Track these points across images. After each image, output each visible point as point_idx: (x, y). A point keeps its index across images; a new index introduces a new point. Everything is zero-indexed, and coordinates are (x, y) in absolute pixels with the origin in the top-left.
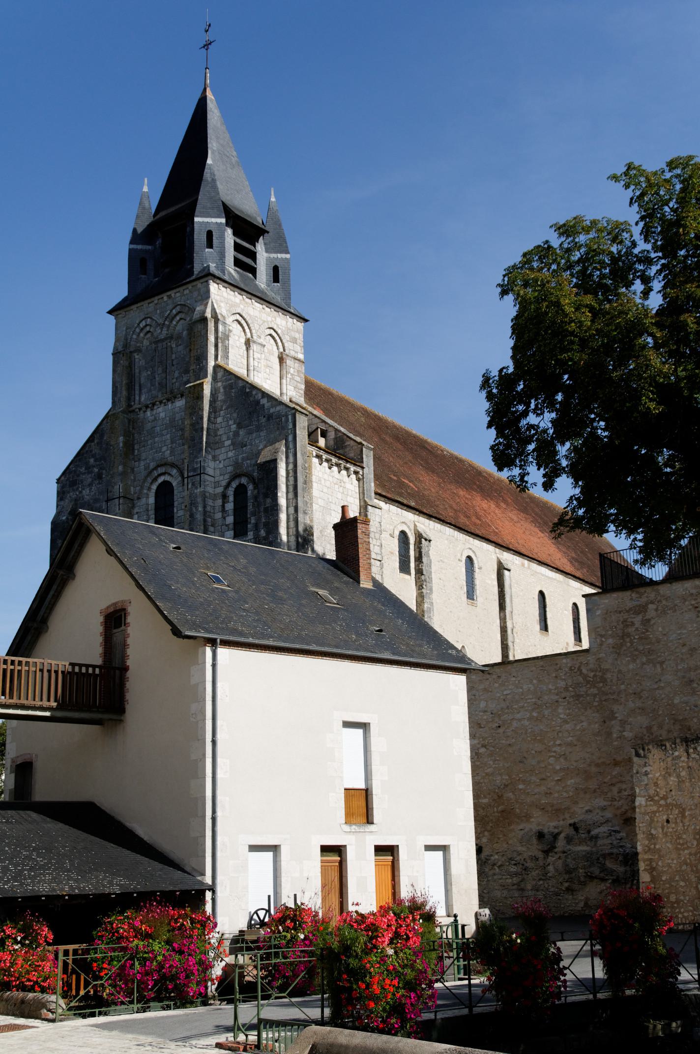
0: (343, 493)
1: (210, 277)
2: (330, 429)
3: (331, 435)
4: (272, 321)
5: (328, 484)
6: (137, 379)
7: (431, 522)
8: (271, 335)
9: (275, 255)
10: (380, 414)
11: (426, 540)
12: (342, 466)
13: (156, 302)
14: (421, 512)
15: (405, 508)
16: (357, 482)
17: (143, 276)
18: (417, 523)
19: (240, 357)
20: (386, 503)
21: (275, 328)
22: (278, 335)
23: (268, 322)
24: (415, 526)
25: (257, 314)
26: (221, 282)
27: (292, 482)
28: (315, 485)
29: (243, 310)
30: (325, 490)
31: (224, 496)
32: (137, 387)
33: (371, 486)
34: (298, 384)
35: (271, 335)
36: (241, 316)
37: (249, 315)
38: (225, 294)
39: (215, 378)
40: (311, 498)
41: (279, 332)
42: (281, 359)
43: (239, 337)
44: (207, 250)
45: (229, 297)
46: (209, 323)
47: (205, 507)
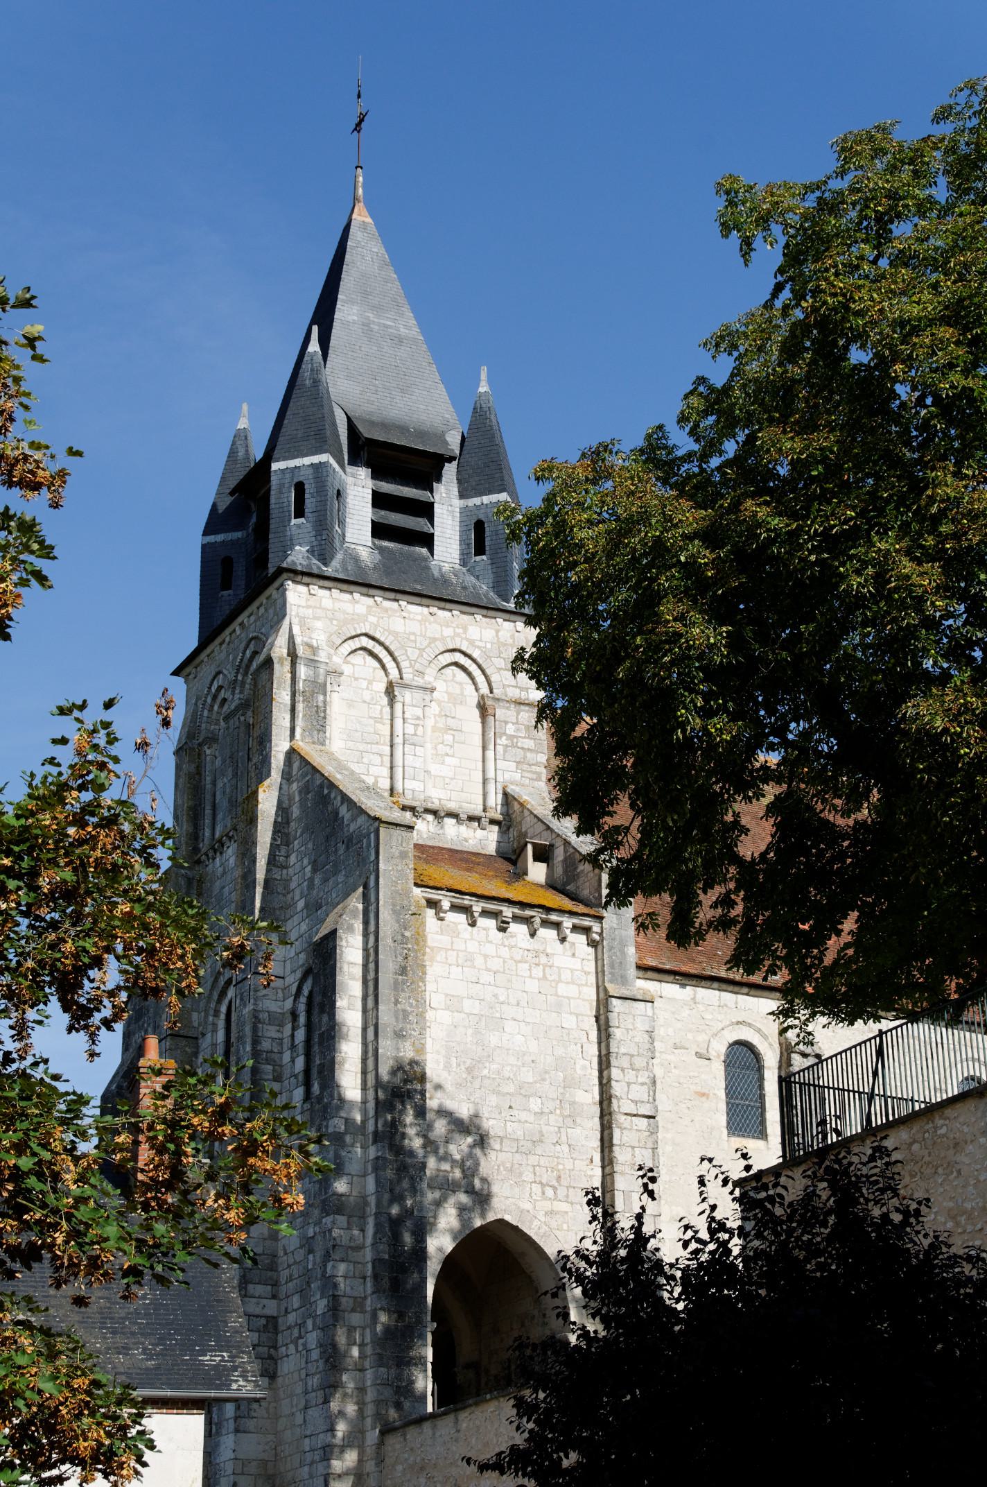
0: (545, 977)
1: (285, 575)
2: (558, 843)
3: (559, 855)
5: (495, 964)
6: (208, 796)
8: (456, 664)
9: (476, 501)
12: (537, 921)
13: (227, 639)
15: (745, 990)
16: (591, 950)
17: (225, 593)
19: (372, 721)
20: (683, 986)
21: (464, 649)
22: (474, 661)
23: (443, 639)
25: (414, 627)
26: (314, 580)
27: (371, 975)
28: (434, 971)
29: (376, 626)
30: (487, 978)
31: (294, 1015)
32: (208, 812)
33: (624, 954)
34: (529, 755)
35: (456, 664)
36: (373, 638)
37: (396, 634)
39: (287, 776)
40: (421, 1002)
41: (475, 655)
42: (483, 709)
43: (370, 682)
44: (294, 521)
45: (338, 605)
46: (276, 666)
47: (256, 1042)
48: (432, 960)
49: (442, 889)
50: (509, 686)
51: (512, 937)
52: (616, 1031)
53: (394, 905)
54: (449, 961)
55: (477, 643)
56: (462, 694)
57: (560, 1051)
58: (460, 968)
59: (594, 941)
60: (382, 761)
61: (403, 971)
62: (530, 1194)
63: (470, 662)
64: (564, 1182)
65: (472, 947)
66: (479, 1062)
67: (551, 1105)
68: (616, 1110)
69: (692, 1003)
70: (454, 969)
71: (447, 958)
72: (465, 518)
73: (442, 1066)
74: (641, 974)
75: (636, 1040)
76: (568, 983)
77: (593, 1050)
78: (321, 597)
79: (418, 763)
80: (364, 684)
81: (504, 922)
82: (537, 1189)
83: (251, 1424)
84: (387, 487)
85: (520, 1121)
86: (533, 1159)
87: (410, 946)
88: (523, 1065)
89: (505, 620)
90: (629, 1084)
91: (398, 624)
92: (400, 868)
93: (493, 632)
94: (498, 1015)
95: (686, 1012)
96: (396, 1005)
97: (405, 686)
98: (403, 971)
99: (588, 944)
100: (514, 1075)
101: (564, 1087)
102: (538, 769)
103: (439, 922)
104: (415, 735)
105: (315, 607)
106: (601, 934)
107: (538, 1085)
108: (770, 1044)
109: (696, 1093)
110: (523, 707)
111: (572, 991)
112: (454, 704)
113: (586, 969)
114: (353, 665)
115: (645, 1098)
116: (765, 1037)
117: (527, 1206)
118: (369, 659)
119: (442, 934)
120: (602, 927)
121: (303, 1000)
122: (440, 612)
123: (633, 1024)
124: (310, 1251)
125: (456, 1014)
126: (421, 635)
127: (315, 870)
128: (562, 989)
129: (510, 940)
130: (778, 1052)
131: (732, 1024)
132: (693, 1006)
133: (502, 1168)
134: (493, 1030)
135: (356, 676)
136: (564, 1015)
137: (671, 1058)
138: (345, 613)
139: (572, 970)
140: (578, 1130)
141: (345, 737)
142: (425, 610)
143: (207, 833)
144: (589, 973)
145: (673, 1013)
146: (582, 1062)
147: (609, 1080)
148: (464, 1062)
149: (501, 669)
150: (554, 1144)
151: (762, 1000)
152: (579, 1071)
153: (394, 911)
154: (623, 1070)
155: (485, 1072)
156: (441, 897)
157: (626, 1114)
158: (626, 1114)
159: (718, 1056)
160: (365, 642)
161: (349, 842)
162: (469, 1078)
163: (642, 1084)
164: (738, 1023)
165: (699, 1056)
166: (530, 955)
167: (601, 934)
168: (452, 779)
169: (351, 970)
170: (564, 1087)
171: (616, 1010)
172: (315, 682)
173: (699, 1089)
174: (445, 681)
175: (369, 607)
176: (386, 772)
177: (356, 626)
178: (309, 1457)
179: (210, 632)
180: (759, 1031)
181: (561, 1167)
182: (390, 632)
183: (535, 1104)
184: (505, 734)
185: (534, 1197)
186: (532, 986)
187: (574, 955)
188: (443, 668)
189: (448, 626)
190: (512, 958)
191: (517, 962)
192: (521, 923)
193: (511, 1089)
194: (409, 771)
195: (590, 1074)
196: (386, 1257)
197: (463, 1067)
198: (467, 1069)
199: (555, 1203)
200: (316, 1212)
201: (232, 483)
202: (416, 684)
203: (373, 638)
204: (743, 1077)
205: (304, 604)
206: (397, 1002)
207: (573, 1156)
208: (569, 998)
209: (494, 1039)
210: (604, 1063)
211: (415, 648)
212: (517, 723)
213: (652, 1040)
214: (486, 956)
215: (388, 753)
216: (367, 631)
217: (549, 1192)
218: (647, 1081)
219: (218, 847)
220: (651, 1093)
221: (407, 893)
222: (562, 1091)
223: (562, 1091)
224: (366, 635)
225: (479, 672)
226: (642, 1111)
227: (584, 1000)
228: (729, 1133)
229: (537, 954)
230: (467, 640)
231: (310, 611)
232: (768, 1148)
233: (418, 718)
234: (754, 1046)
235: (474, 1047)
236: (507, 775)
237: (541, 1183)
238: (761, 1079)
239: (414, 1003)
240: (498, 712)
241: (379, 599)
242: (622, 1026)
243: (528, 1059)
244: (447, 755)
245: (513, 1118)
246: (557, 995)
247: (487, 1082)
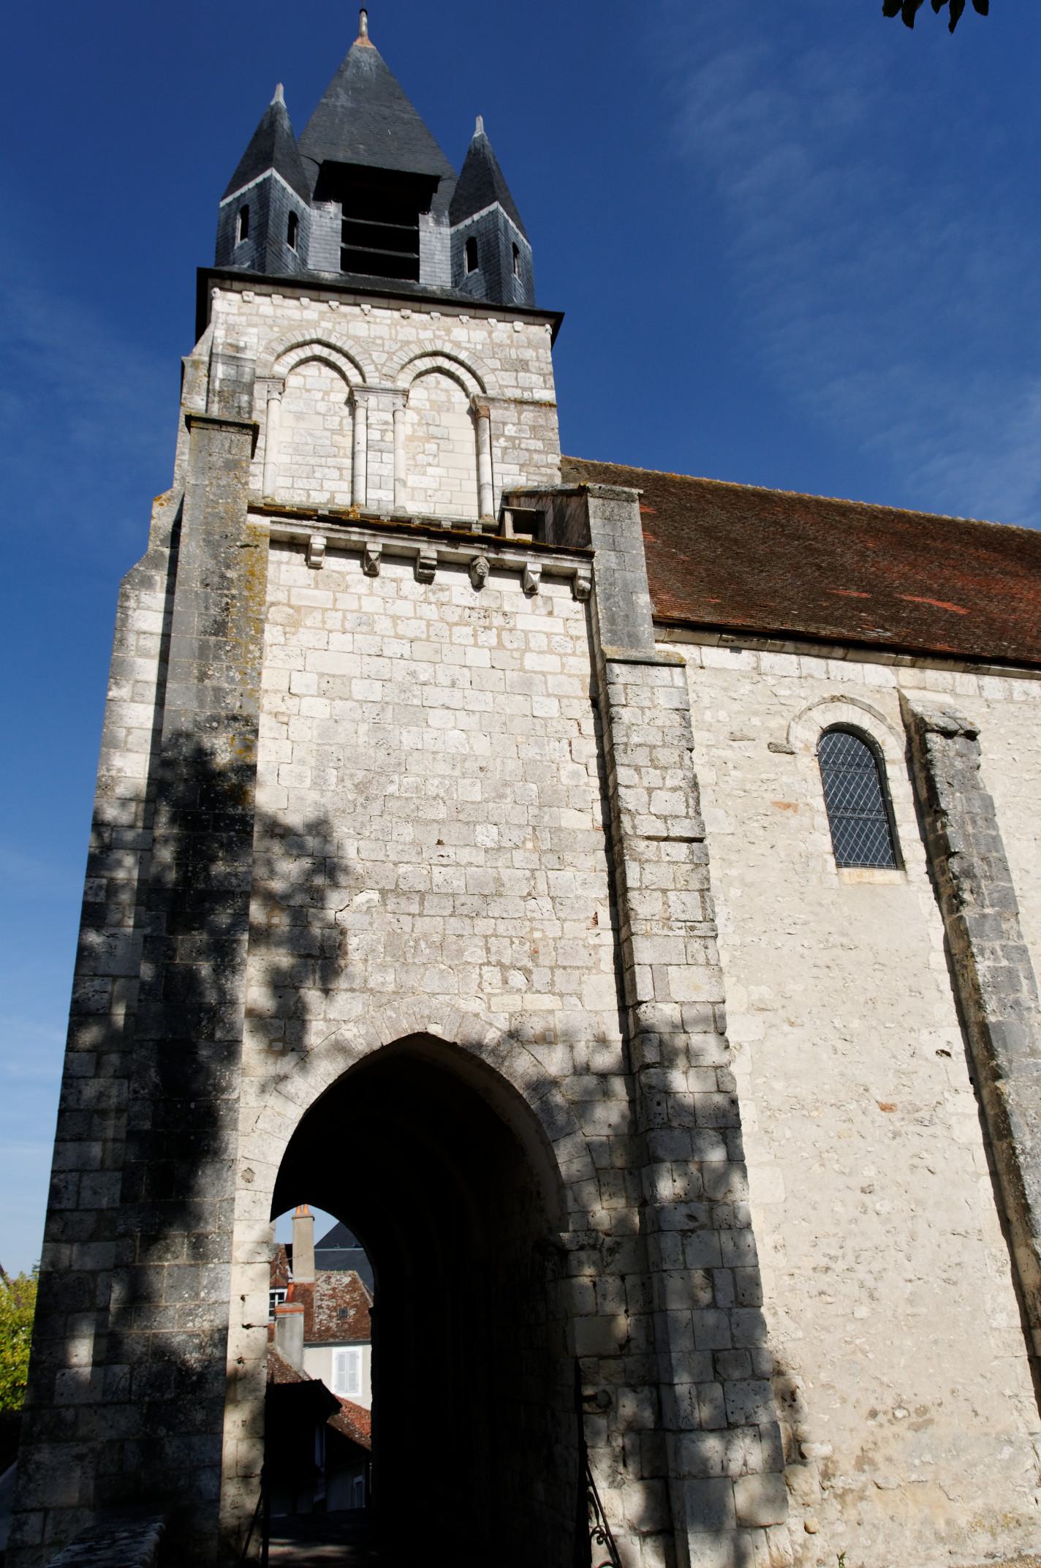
0: (500, 645)
7: (988, 681)
10: (973, 520)
11: (948, 734)
14: (922, 655)
15: (839, 652)
16: (579, 606)
18: (904, 692)
19: (328, 434)
20: (737, 649)
21: (447, 350)
22: (462, 364)
23: (420, 342)
24: (903, 701)
29: (330, 332)
30: (394, 648)
33: (631, 604)
34: (536, 456)
37: (356, 339)
41: (463, 356)
43: (326, 393)
45: (279, 312)
49: (309, 518)
50: (507, 387)
51: (442, 590)
52: (623, 711)
53: (208, 533)
54: (327, 626)
55: (464, 345)
56: (449, 401)
57: (530, 752)
58: (349, 636)
59: (583, 592)
60: (341, 475)
61: (220, 628)
62: (480, 985)
63: (456, 366)
64: (545, 960)
65: (371, 605)
66: (380, 774)
67: (516, 836)
68: (630, 831)
69: (754, 674)
70: (335, 637)
71: (324, 622)
73: (308, 782)
74: (663, 633)
75: (659, 722)
76: (540, 652)
77: (591, 748)
78: (259, 305)
79: (386, 470)
80: (319, 395)
81: (424, 566)
82: (492, 974)
85: (458, 864)
86: (483, 926)
87: (234, 592)
88: (464, 775)
89: (498, 321)
90: (650, 791)
92: (223, 482)
93: (485, 334)
94: (416, 702)
95: (746, 688)
96: (201, 679)
97: (367, 390)
98: (220, 628)
99: (575, 599)
100: (447, 791)
101: (540, 807)
102: (549, 471)
103: (313, 572)
104: (382, 440)
105: (250, 314)
106: (591, 581)
107: (491, 805)
108: (890, 728)
109: (775, 804)
110: (525, 407)
111: (551, 663)
112: (438, 413)
113: (574, 632)
114: (304, 377)
115: (681, 810)
116: (880, 717)
117: (475, 1006)
118: (327, 371)
119: (317, 587)
120: (592, 570)
122: (416, 316)
123: (651, 700)
125: (338, 702)
126: (391, 339)
128: (531, 661)
129: (440, 594)
130: (905, 739)
131: (824, 701)
132: (758, 678)
133: (423, 945)
134: (407, 724)
135: (308, 387)
136: (535, 698)
137: (728, 754)
138: (289, 319)
139: (548, 635)
140: (568, 874)
141: (291, 451)
142: (396, 314)
144: (578, 638)
145: (726, 689)
146: (572, 766)
147: (616, 785)
148: (352, 775)
149: (496, 370)
150: (524, 898)
151: (868, 666)
152: (565, 780)
153: (208, 542)
154: (637, 769)
155: (392, 789)
156: (308, 531)
157: (648, 838)
158: (648, 838)
159: (807, 748)
160: (318, 350)
162: (361, 800)
163: (674, 789)
164: (834, 699)
165: (774, 748)
166: (474, 614)
167: (591, 581)
168: (436, 490)
169: (142, 642)
170: (540, 807)
171: (621, 680)
172: (237, 382)
173: (779, 798)
174: (426, 388)
175: (321, 313)
176: (346, 486)
177: (304, 332)
180: (869, 709)
181: (537, 935)
182: (349, 336)
183: (487, 836)
184: (503, 435)
185: (488, 990)
187: (550, 613)
188: (416, 358)
189: (425, 329)
190: (442, 620)
191: (451, 625)
192: (458, 571)
193: (442, 813)
195: (587, 784)
196: (147, 1125)
197: (348, 783)
198: (356, 786)
199: (529, 996)
202: (382, 386)
204: (853, 778)
205: (236, 312)
207: (561, 914)
208: (544, 674)
209: (408, 739)
210: (606, 764)
211: (383, 351)
212: (519, 423)
213: (688, 725)
214: (395, 618)
215: (350, 466)
216: (319, 337)
217: (517, 979)
218: (683, 784)
220: (691, 802)
222: (536, 811)
223: (536, 811)
224: (319, 342)
225: (469, 376)
226: (675, 832)
227: (570, 676)
228: (839, 865)
230: (450, 341)
231: (243, 319)
232: (908, 882)
233: (386, 423)
234: (864, 732)
235: (371, 752)
237: (500, 964)
238: (883, 779)
239: (238, 677)
240: (493, 413)
241: (334, 304)
242: (632, 703)
243: (472, 766)
244: (430, 465)
245: (444, 861)
246: (522, 669)
247: (392, 804)
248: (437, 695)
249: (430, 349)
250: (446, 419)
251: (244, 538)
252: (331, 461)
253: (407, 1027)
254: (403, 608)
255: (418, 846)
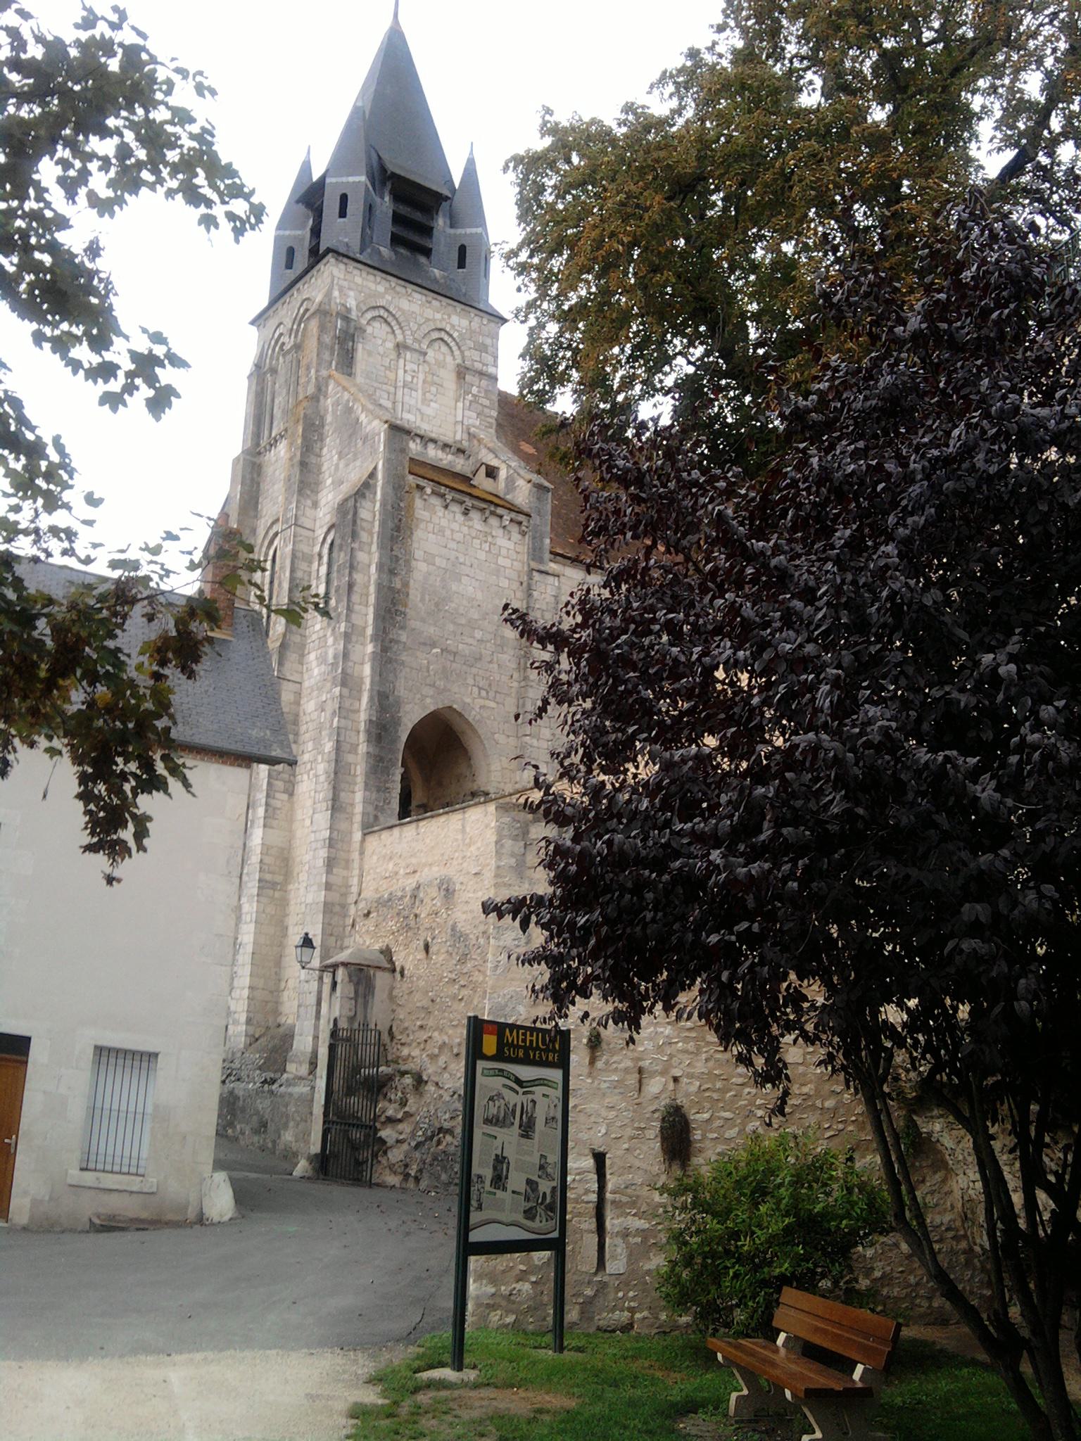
0: (490, 551)
4: (443, 319)
5: (458, 536)
23: (434, 320)
25: (415, 308)
28: (419, 534)
30: (453, 545)
33: (542, 542)
35: (442, 339)
36: (387, 310)
38: (358, 280)
41: (455, 335)
43: (384, 341)
48: (417, 526)
65: (444, 522)
67: (488, 637)
72: (261, 983)
79: (413, 402)
80: (380, 342)
82: (475, 690)
83: (275, 823)
84: (404, 210)
86: (474, 670)
91: (405, 304)
117: (468, 700)
118: (384, 325)
121: (327, 546)
124: (323, 710)
127: (340, 458)
128: (501, 561)
143: (266, 433)
161: (365, 439)
178: (314, 845)
179: (280, 295)
182: (400, 309)
183: (478, 634)
186: (482, 556)
193: (463, 621)
194: (406, 407)
200: (329, 684)
201: (297, 196)
203: (387, 310)
206: (392, 550)
209: (454, 587)
217: (483, 693)
219: (273, 443)
221: (403, 477)
229: (486, 534)
236: (471, 421)
246: (496, 563)
248: (466, 570)
249: (439, 326)
250: (442, 373)
251: (407, 489)
252: (384, 387)
253: (447, 704)
254: (455, 526)
255: (454, 633)
